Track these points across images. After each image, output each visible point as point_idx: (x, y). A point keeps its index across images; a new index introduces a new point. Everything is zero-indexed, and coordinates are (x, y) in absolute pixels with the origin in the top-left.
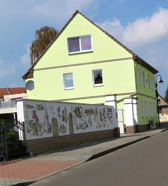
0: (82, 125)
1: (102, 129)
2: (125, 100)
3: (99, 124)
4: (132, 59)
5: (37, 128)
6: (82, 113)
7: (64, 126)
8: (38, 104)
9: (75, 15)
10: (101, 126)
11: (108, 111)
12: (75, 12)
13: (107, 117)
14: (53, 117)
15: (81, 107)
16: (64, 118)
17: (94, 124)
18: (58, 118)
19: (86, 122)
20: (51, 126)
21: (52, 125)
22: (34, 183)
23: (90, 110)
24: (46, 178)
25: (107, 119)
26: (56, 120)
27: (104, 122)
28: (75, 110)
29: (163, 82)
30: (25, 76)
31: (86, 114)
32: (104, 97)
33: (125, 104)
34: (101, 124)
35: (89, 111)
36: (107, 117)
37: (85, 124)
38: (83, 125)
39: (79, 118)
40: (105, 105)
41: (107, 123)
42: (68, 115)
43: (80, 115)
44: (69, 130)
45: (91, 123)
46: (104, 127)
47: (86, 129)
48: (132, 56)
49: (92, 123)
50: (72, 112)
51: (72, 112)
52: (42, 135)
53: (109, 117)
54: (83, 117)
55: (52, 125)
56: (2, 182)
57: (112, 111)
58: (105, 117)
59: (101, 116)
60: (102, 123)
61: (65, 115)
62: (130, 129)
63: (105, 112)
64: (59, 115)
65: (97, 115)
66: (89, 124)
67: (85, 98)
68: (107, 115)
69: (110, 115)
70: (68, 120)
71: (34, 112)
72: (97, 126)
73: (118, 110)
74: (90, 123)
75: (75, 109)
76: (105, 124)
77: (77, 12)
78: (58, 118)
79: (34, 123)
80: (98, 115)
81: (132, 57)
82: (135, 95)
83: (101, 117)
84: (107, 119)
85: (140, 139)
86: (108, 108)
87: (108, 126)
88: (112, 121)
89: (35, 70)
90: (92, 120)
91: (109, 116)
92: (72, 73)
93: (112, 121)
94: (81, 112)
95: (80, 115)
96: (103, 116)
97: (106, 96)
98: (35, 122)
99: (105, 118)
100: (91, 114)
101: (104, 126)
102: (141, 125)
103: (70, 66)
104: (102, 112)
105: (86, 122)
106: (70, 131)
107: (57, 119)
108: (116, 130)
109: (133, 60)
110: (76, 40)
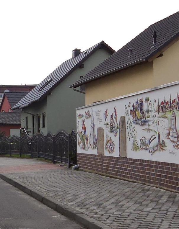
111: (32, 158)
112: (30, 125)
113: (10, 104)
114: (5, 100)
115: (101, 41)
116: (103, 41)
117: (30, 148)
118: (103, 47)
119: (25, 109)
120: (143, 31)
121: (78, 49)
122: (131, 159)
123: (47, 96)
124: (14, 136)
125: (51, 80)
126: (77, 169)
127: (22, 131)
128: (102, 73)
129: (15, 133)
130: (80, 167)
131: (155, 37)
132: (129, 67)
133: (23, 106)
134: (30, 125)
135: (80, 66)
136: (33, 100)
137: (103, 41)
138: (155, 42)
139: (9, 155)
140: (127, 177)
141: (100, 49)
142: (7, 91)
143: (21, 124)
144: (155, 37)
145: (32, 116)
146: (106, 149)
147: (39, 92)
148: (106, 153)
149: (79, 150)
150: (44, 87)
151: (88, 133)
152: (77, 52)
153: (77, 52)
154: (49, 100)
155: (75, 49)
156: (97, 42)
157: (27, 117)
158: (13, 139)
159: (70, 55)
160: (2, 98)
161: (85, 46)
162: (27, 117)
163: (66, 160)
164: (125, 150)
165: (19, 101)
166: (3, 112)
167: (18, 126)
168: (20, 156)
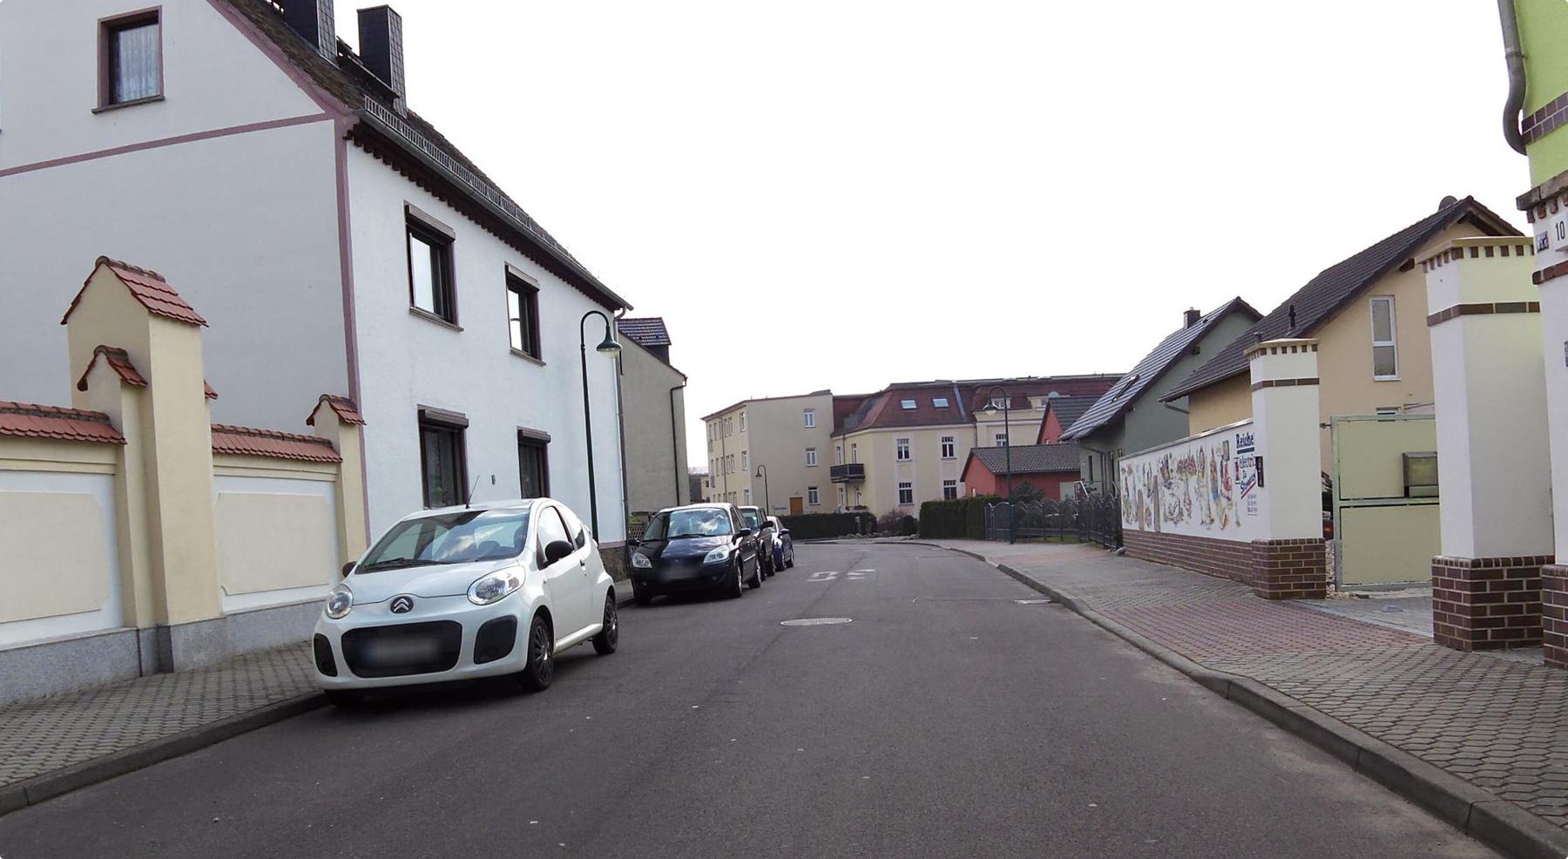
1: (1215, 533)
3: (1208, 512)
11: (1239, 452)
13: (1238, 479)
14: (925, 501)
17: (1198, 514)
25: (1236, 490)
27: (1224, 502)
29: (545, 364)
33: (493, 483)
34: (1214, 515)
36: (1238, 479)
41: (1234, 508)
45: (1188, 507)
46: (1224, 526)
53: (1245, 481)
58: (1227, 482)
60: (1219, 508)
68: (1237, 470)
73: (1009, 468)
82: (320, 469)
83: (1214, 480)
84: (1236, 490)
86: (1241, 436)
87: (1238, 524)
90: (1193, 497)
91: (1245, 477)
96: (1222, 476)
99: (1228, 488)
100: (1189, 475)
104: (1218, 460)
110: (383, 10)
111: (1082, 542)
112: (1097, 475)
113: (1061, 426)
114: (1049, 419)
115: (1235, 298)
116: (1239, 298)
117: (1077, 523)
118: (1238, 308)
119: (1085, 440)
120: (1280, 305)
121: (1196, 309)
122: (1167, 535)
123: (1126, 417)
124: (884, 518)
125: (1138, 378)
126: (1122, 554)
127: (1079, 487)
128: (1209, 379)
129: (1067, 490)
130: (1125, 550)
131: (1292, 315)
132: (1238, 375)
133: (1079, 434)
134: (1097, 475)
135: (1192, 349)
136: (1096, 423)
137: (1239, 298)
138: (1293, 325)
139: (1043, 539)
140: (1198, 567)
141: (1234, 312)
142: (1054, 394)
143: (1079, 472)
144: (1292, 315)
145: (1099, 455)
146: (1166, 520)
147: (1113, 404)
148: (1146, 529)
149: (1125, 526)
150: (1128, 388)
151: (1131, 498)
152: (1193, 316)
153: (1193, 316)
154: (1131, 423)
155: (1189, 309)
156: (1231, 298)
157: (1090, 457)
158: (1065, 507)
159: (1179, 323)
160: (1041, 422)
161: (1209, 306)
162: (1090, 457)
163: (948, 498)
164: (1159, 522)
165: (1075, 421)
166: (1047, 443)
167: (1073, 475)
168: (1062, 540)
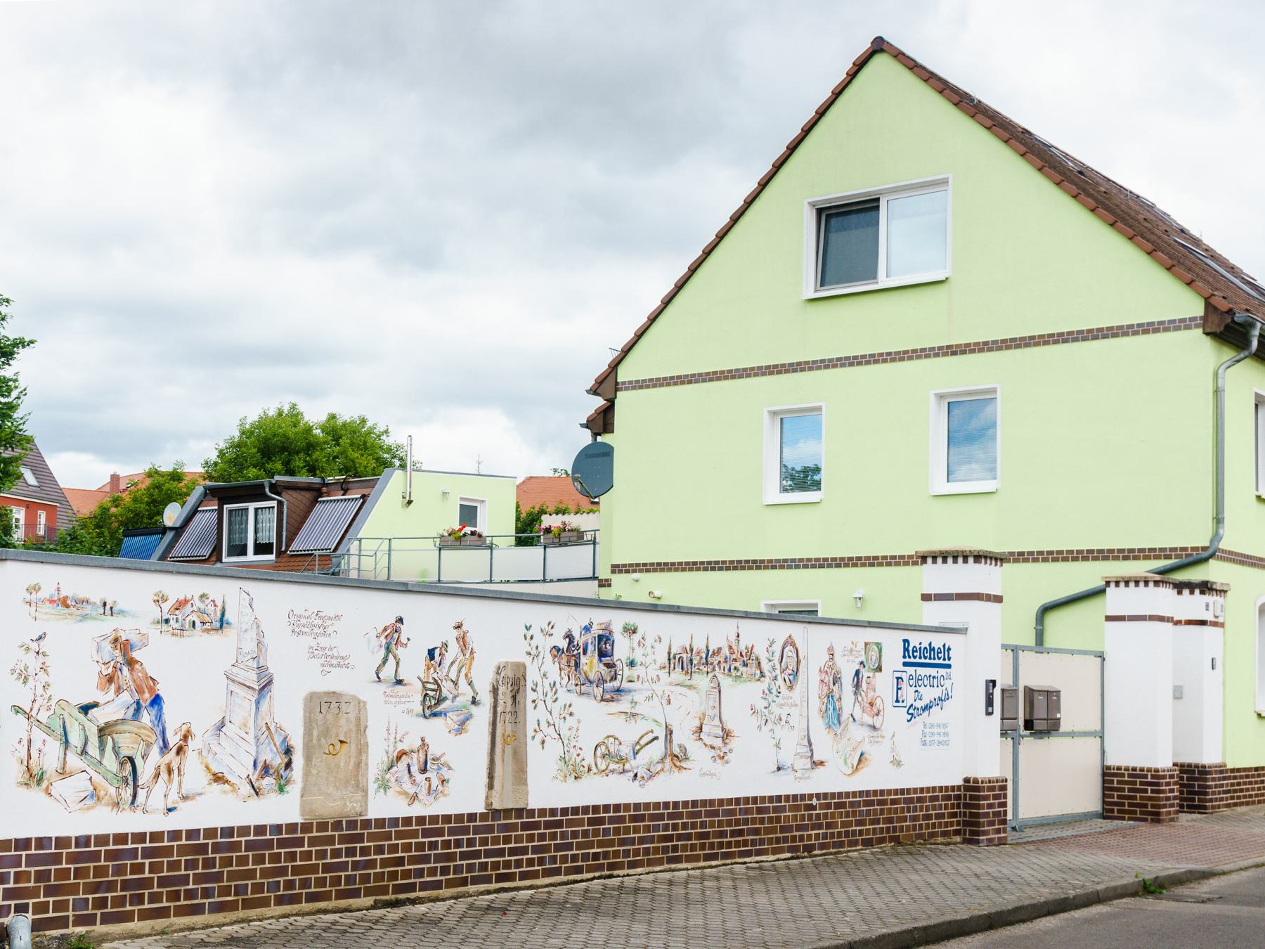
0: (625, 750)
2: (1111, 590)
4: (1201, 330)
5: (131, 760)
6: (635, 672)
7: (434, 751)
8: (166, 592)
9: (860, 65)
10: (817, 764)
11: (905, 664)
12: (866, 45)
15: (631, 631)
16: (440, 700)
18: (374, 697)
19: (669, 733)
20: (288, 751)
21: (297, 742)
22: (1223, 877)
23: (726, 651)
24: (1253, 869)
26: (351, 709)
27: (857, 733)
28: (564, 644)
30: (601, 416)
31: (678, 675)
32: (915, 563)
35: (715, 660)
37: (660, 744)
38: (636, 753)
39: (602, 700)
40: (820, 615)
42: (483, 677)
43: (614, 678)
44: (485, 780)
45: (718, 743)
47: (657, 779)
48: (1194, 307)
49: (734, 743)
50: (527, 660)
51: (527, 660)
52: (182, 806)
54: (638, 697)
55: (297, 742)
56: (1192, 838)
57: (949, 666)
59: (830, 695)
61: (453, 676)
62: (1130, 790)
63: (879, 669)
64: (388, 672)
65: (791, 688)
66: (695, 749)
67: (880, 565)
69: (929, 694)
70: (482, 716)
71: (124, 647)
72: (787, 758)
74: (708, 741)
75: (569, 636)
76: (866, 747)
77: (879, 47)
78: (374, 697)
79: (102, 723)
80: (799, 687)
81: (1202, 314)
85: (1017, 910)
88: (946, 734)
89: (627, 389)
92: (819, 409)
93: (941, 730)
94: (632, 664)
95: (616, 684)
97: (924, 559)
98: (120, 716)
101: (860, 760)
102: (1232, 770)
103: (811, 369)
105: (669, 733)
106: (491, 786)
107: (361, 705)
108: (972, 798)
109: (1207, 334)
